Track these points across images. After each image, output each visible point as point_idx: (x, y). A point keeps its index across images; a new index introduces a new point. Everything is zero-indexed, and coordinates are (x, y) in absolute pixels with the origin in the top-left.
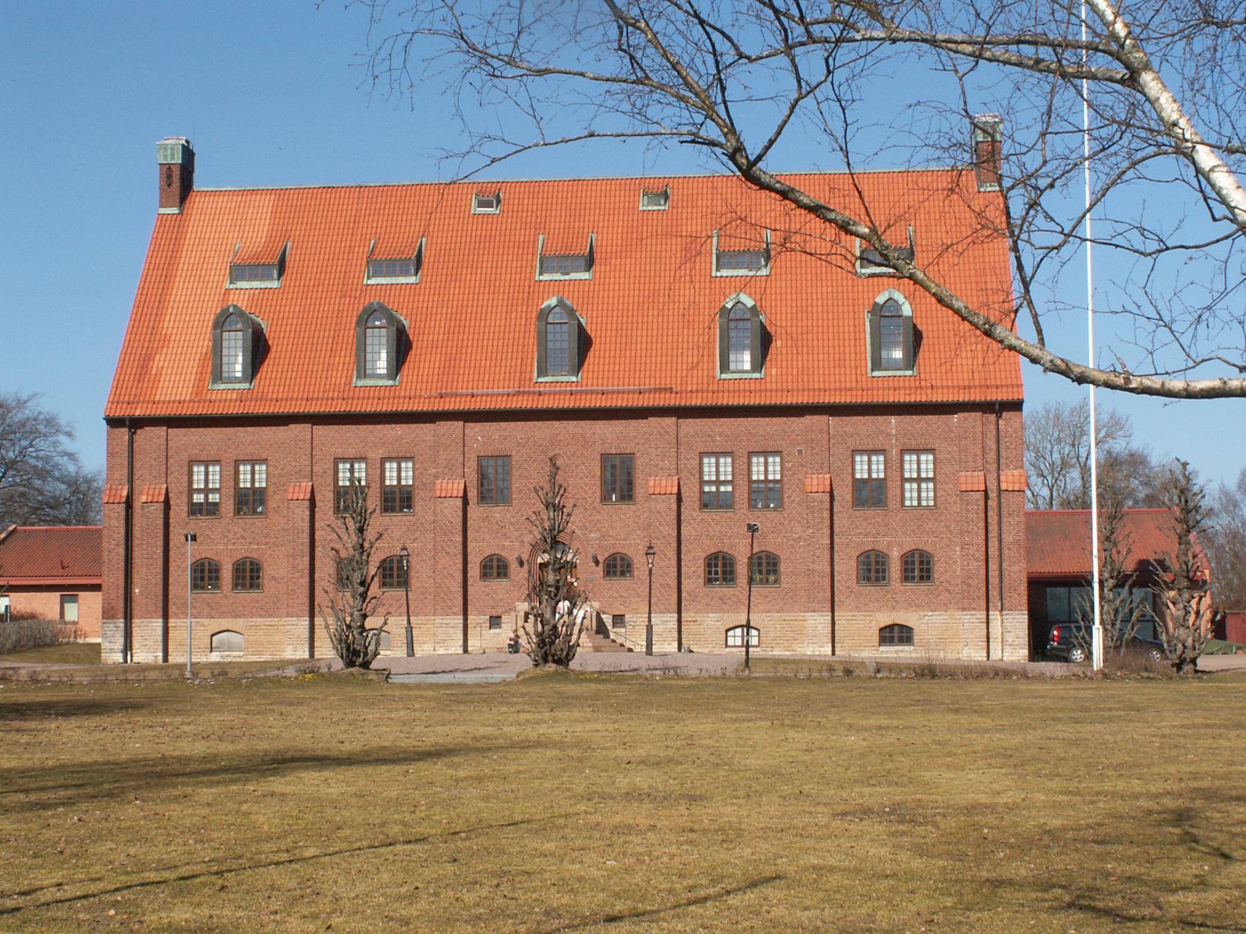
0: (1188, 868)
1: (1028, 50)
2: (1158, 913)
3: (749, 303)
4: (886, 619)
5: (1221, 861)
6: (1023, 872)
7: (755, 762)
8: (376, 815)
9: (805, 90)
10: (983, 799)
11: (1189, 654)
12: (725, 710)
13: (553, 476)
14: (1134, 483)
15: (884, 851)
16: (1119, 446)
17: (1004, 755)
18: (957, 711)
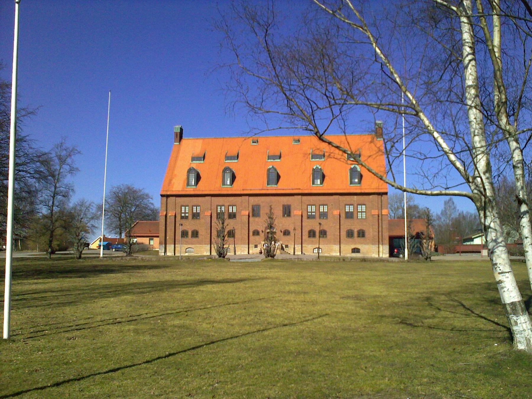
0: (430, 312)
1: (391, 107)
2: (422, 325)
3: (320, 167)
4: (353, 246)
5: (438, 311)
6: (388, 313)
7: (320, 283)
8: (226, 296)
9: (334, 117)
10: (378, 294)
11: (429, 256)
12: (313, 270)
13: (271, 210)
14: (415, 213)
15: (353, 308)
16: (411, 204)
17: (383, 282)
18: (371, 270)
